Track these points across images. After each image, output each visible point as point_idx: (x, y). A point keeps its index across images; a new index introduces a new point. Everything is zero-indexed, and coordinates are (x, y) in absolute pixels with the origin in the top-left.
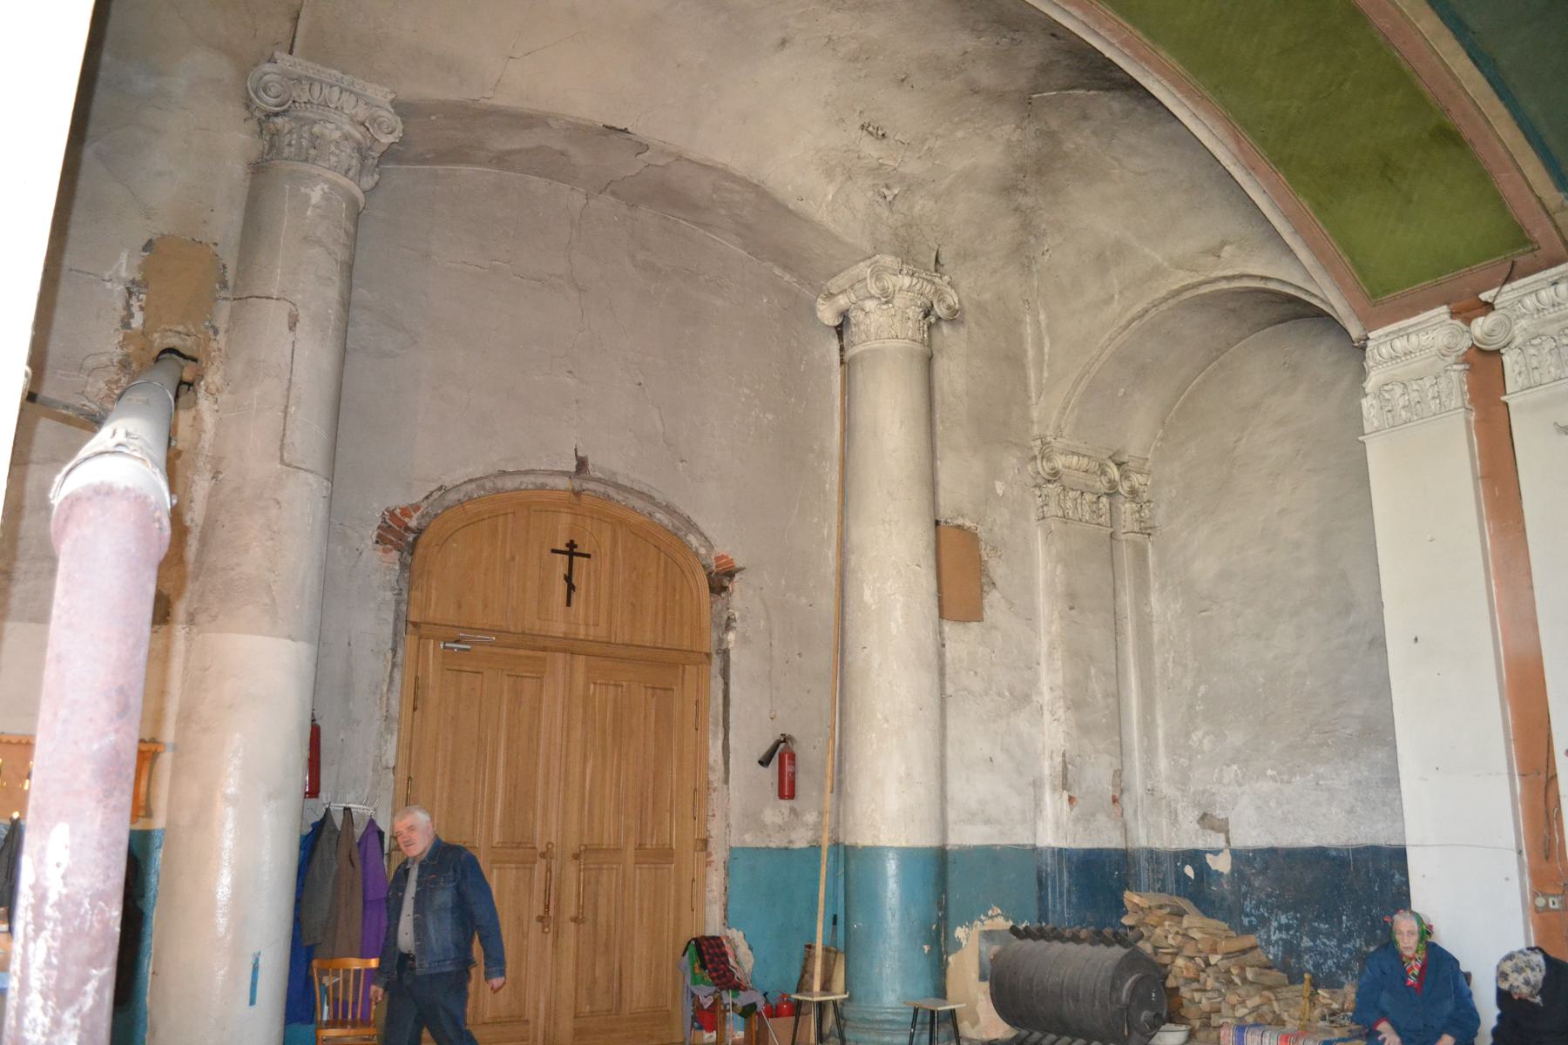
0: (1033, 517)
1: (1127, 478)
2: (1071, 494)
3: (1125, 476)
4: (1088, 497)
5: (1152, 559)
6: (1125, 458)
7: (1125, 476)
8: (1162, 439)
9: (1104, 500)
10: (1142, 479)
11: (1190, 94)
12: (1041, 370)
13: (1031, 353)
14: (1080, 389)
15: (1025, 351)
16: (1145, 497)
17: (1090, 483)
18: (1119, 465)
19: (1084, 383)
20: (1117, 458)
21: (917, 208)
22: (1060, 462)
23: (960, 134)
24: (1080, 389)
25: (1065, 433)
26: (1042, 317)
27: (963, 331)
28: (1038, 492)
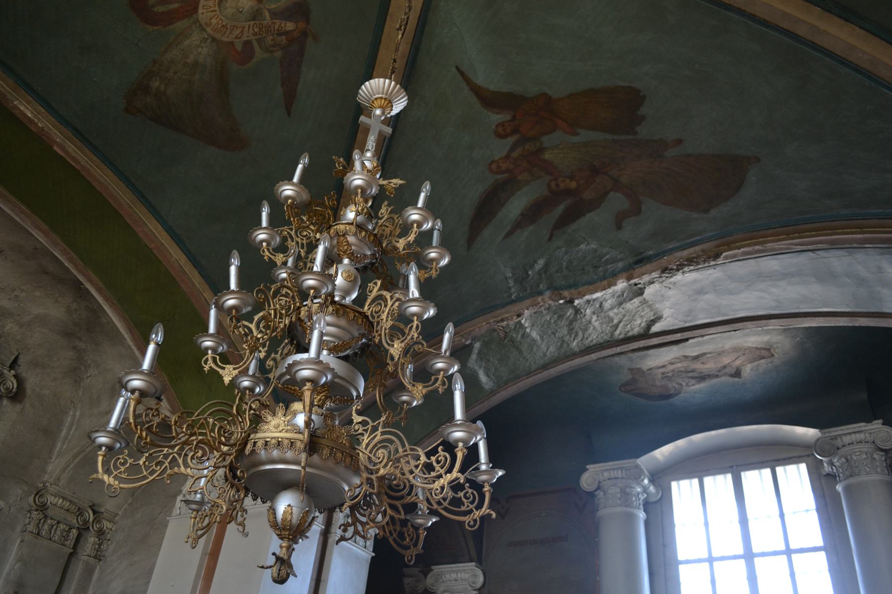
0: (19, 529)
1: (99, 522)
2: (49, 521)
3: (97, 520)
4: (62, 526)
5: (96, 576)
6: (102, 510)
7: (97, 520)
8: (130, 504)
9: (74, 531)
10: (109, 525)
11: (462, 408)
12: (64, 444)
13: (64, 433)
14: (78, 459)
15: (62, 430)
16: (108, 537)
17: (69, 519)
18: (94, 512)
19: (81, 456)
20: (96, 508)
21: (7, 328)
22: (51, 499)
23: (37, 294)
24: (78, 459)
25: (60, 484)
26: (78, 413)
27: (18, 407)
28: (28, 515)
